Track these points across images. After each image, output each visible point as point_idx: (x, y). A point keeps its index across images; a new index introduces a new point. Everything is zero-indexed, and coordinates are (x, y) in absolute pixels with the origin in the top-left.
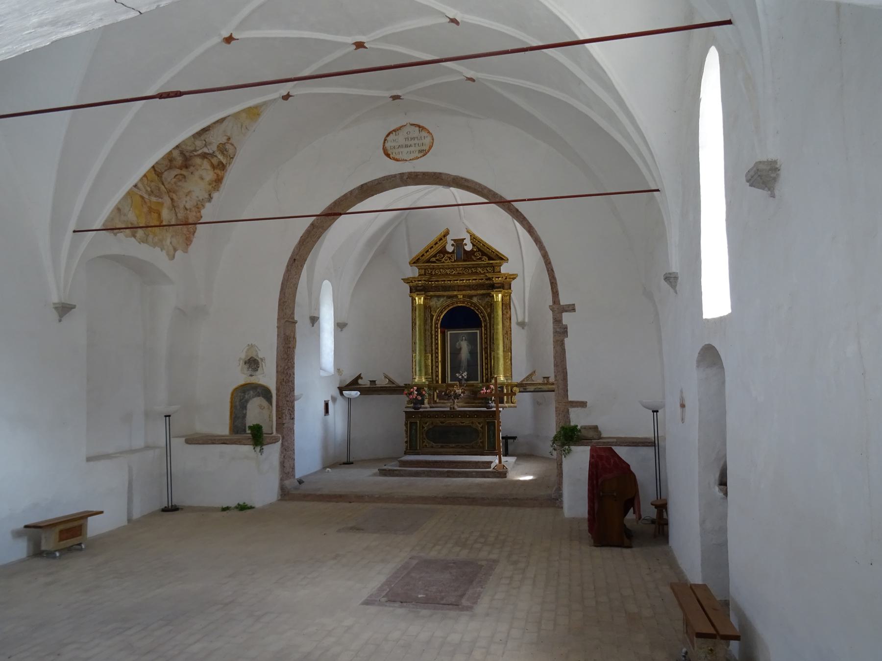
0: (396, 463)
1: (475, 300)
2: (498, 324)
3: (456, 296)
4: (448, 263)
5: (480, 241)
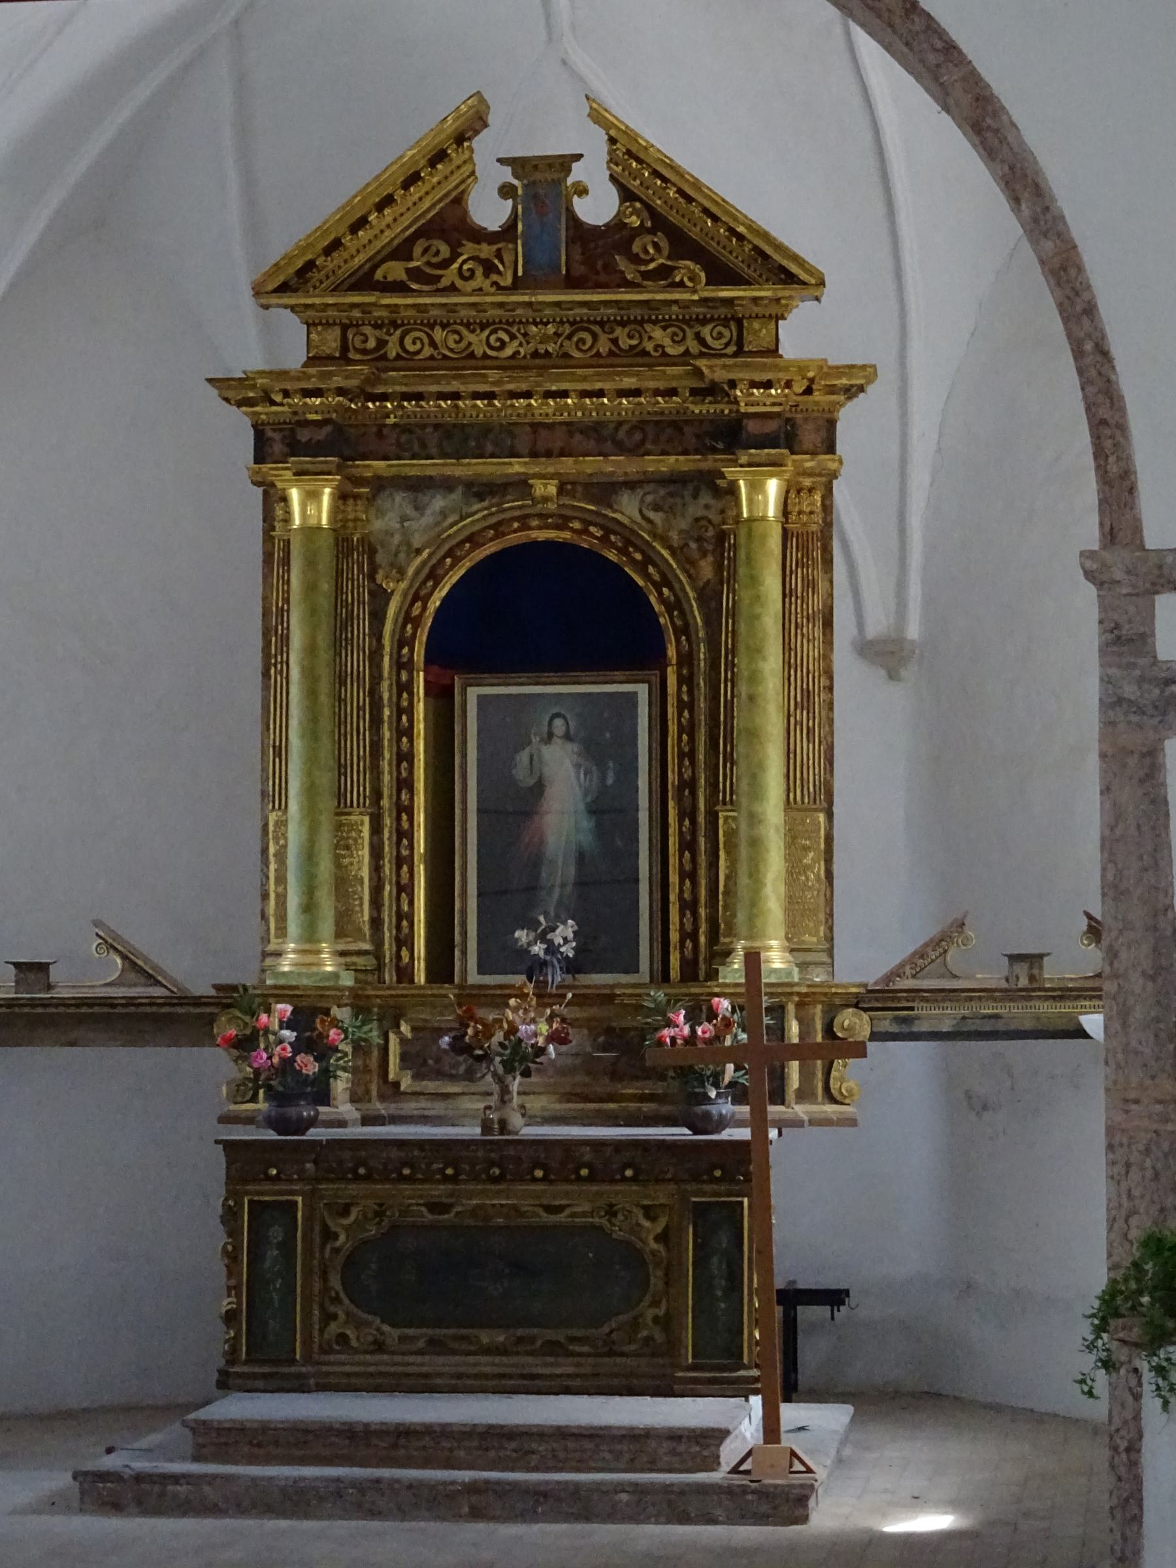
0: (173, 1433)
1: (628, 509)
2: (757, 651)
3: (522, 485)
4: (478, 294)
5: (664, 173)
